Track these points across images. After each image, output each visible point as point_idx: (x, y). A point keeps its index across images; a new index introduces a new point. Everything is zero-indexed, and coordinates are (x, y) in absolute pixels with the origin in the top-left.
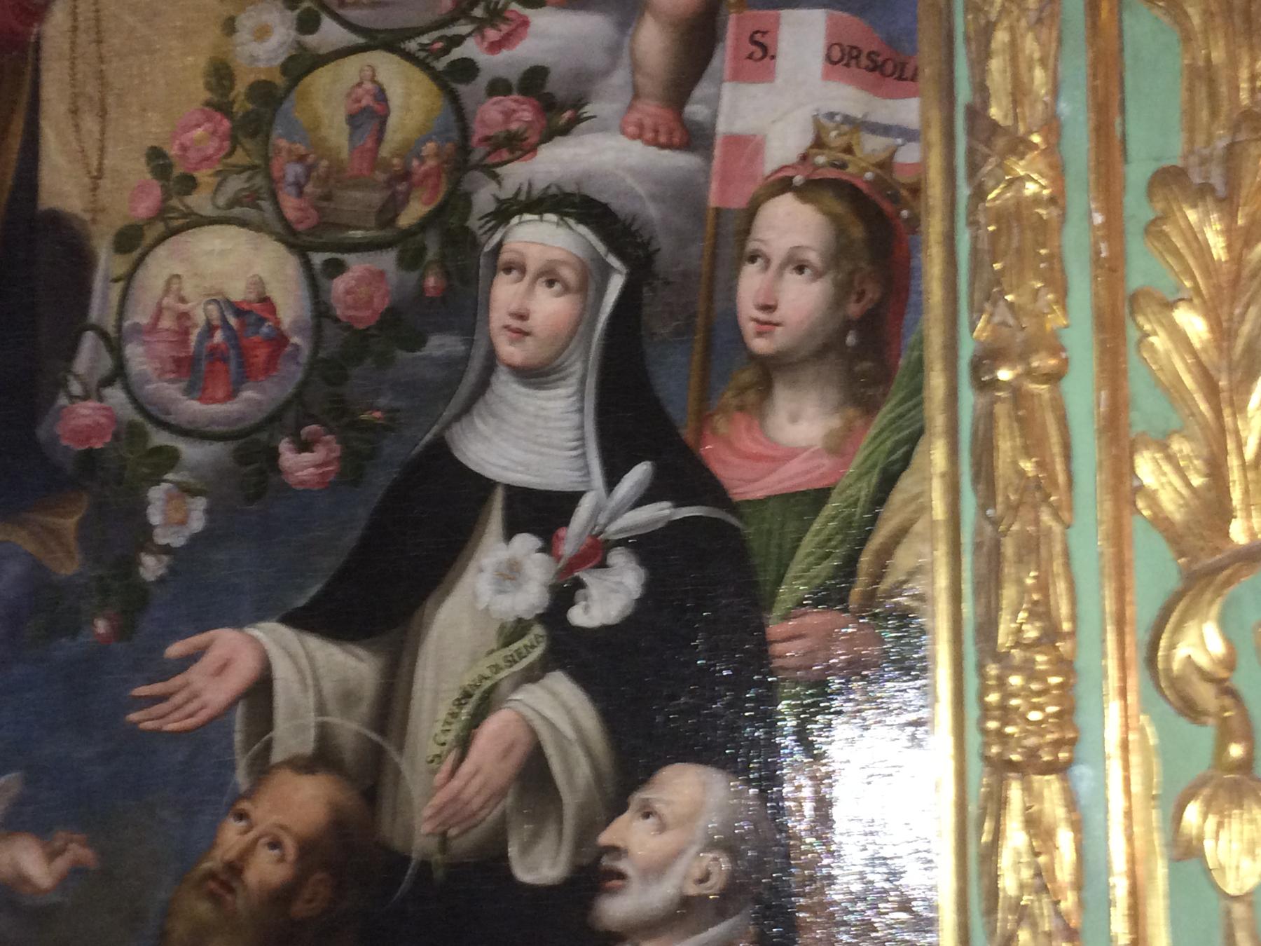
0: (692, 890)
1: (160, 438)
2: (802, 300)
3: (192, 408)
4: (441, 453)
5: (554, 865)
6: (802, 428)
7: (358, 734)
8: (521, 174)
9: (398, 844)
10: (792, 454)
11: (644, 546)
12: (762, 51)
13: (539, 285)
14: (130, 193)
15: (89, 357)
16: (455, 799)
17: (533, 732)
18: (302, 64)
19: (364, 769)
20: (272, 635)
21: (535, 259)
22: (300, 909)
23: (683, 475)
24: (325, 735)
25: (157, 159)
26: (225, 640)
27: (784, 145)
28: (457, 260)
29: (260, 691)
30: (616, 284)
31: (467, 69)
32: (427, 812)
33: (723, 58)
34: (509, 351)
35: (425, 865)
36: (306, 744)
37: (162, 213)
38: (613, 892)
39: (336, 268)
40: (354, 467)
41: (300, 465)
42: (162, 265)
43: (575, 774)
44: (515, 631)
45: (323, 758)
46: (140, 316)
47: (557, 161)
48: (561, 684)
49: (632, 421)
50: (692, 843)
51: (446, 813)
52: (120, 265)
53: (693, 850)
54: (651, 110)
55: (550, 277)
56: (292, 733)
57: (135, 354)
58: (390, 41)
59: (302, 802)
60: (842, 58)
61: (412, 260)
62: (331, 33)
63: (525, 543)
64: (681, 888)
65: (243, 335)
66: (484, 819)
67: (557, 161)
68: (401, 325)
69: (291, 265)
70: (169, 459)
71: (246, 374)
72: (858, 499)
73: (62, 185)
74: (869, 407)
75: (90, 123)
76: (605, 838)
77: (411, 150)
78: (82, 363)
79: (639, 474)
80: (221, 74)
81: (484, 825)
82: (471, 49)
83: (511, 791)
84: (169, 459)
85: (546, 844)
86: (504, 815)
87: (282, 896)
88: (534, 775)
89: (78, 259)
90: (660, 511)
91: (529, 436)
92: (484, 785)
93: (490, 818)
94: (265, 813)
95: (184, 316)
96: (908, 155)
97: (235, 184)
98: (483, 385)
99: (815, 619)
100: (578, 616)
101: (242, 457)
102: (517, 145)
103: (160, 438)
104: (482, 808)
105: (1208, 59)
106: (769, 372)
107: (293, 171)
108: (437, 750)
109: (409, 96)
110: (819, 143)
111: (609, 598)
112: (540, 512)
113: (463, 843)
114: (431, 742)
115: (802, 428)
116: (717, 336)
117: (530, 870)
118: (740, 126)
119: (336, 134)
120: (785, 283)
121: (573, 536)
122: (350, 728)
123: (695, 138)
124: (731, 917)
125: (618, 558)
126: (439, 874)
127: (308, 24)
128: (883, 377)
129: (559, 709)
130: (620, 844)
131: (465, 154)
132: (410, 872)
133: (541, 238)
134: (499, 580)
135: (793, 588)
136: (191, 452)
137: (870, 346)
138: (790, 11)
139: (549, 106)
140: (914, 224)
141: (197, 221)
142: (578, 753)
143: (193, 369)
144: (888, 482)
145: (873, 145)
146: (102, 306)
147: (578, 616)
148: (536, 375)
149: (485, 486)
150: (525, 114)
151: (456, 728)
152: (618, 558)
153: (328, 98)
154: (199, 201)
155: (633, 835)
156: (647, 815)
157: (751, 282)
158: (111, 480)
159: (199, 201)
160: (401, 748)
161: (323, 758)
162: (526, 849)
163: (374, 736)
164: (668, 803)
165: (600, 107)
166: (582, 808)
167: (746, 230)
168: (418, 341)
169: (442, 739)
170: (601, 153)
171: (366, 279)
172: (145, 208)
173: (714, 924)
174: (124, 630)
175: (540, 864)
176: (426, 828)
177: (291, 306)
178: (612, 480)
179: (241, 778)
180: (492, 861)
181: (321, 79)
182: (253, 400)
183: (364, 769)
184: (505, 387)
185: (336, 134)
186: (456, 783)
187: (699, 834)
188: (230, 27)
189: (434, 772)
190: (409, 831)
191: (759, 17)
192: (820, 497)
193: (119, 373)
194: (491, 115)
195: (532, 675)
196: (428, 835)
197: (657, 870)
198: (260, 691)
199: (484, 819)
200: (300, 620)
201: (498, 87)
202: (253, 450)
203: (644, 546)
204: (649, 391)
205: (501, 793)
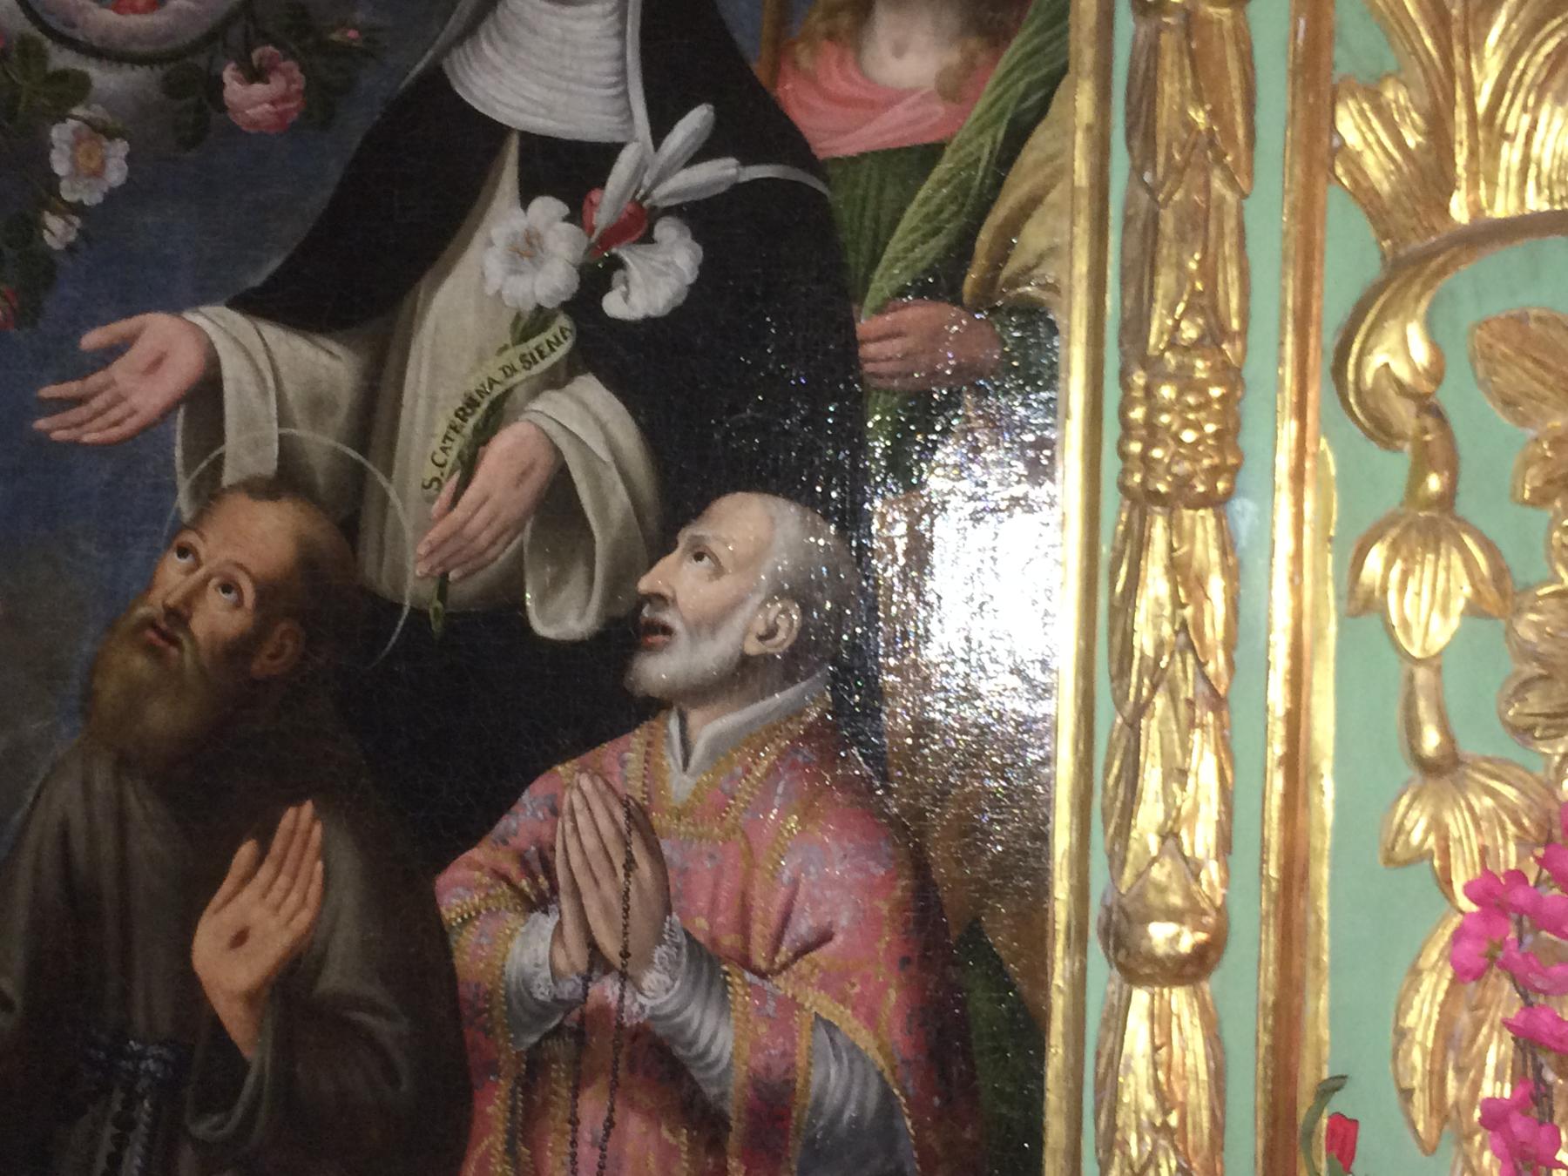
1: (61, 59)
10: (895, 97)
11: (699, 215)
19: (344, 498)
20: (219, 323)
23: (753, 124)
24: (288, 451)
26: (157, 328)
29: (205, 396)
36: (267, 461)
40: (323, 102)
41: (250, 99)
44: (534, 322)
45: (287, 480)
48: (590, 389)
56: (248, 448)
59: (263, 535)
63: (547, 209)
70: (78, 87)
74: (997, 37)
79: (695, 121)
84: (74, 88)
87: (238, 651)
88: (556, 505)
90: (722, 171)
99: (917, 313)
100: (614, 305)
101: (173, 88)
103: (61, 59)
111: (655, 281)
112: (567, 169)
121: (608, 202)
122: (322, 444)
125: (667, 231)
129: (589, 422)
134: (513, 257)
136: (104, 78)
147: (614, 305)
149: (496, 132)
152: (667, 231)
155: (680, 580)
161: (287, 480)
175: (564, 615)
178: (660, 131)
179: (184, 504)
180: (503, 611)
192: (930, 154)
195: (555, 380)
197: (710, 624)
198: (205, 396)
200: (253, 304)
203: (699, 215)
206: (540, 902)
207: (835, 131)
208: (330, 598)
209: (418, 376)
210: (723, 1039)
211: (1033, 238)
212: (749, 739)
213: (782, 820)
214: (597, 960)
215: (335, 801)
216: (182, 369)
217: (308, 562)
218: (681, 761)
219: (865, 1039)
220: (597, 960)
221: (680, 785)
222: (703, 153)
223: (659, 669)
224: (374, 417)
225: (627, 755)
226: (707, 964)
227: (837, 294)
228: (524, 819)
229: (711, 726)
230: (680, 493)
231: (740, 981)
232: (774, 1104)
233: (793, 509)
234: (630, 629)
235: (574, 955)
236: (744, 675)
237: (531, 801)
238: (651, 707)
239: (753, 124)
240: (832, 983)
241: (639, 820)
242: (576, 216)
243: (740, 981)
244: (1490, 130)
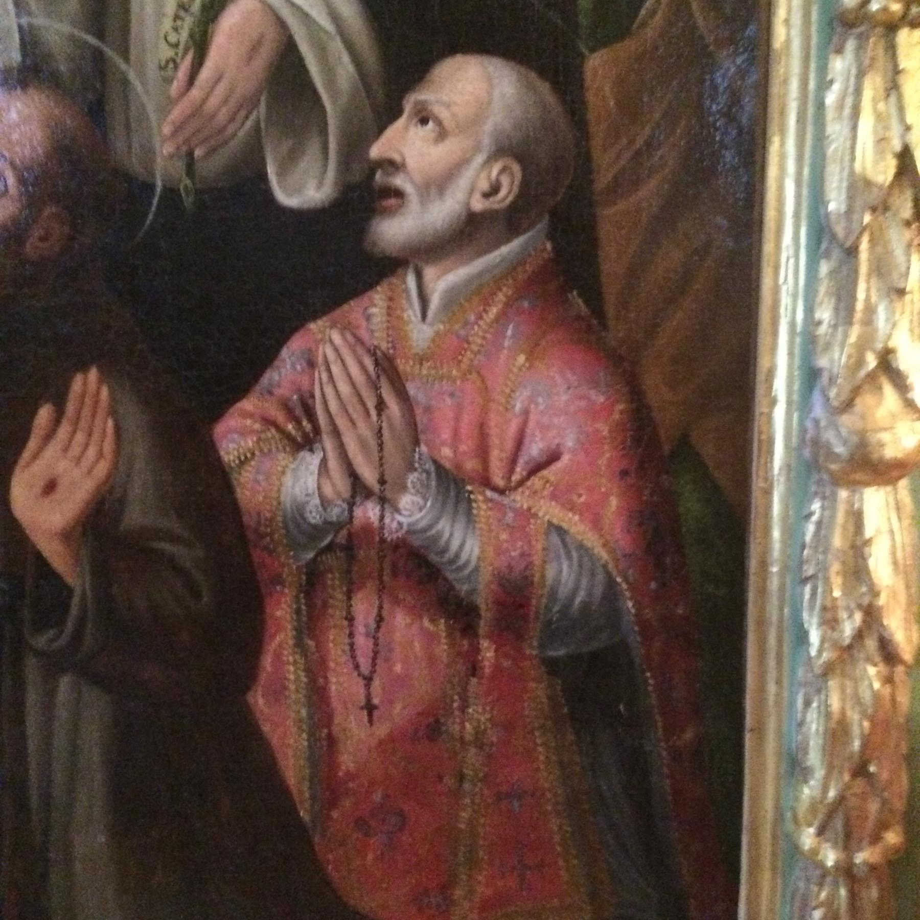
0: (478, 205)
5: (320, 185)
7: (72, 38)
9: (135, 166)
16: (197, 111)
17: (282, 24)
22: (32, 247)
32: (167, 130)
35: (171, 193)
38: (389, 212)
43: (335, 75)
47: (852, 791)
50: (477, 149)
51: (189, 130)
53: (480, 159)
64: (468, 204)
66: (234, 135)
72: (127, 60)
76: (376, 151)
81: (232, 143)
83: (263, 99)
85: (309, 162)
86: (257, 129)
88: (286, 78)
92: (231, 91)
93: (241, 134)
104: (232, 120)
108: (169, 53)
113: (211, 166)
114: (163, 44)
117: (289, 194)
124: (525, 231)
126: (188, 202)
130: (397, 157)
132: (155, 201)
142: (337, 46)
151: (188, 23)
155: (409, 146)
156: (424, 121)
160: (125, 53)
162: (289, 162)
163: (92, 40)
164: (448, 106)
166: (347, 118)
169: (173, 38)
173: (508, 240)
175: (304, 186)
176: (167, 149)
180: (246, 185)
186: (196, 93)
187: (487, 141)
189: (169, 81)
190: (149, 153)
196: (171, 157)
197: (438, 185)
199: (234, 135)
205: (251, 103)
206: (306, 442)
210: (471, 547)
214: (359, 489)
217: (63, 151)
218: (419, 312)
219: (592, 540)
221: (421, 334)
223: (394, 230)
225: (376, 302)
226: (452, 486)
228: (285, 371)
229: (443, 280)
231: (481, 500)
234: (366, 193)
235: (339, 484)
236: (470, 232)
238: (387, 266)
241: (386, 368)
243: (481, 500)
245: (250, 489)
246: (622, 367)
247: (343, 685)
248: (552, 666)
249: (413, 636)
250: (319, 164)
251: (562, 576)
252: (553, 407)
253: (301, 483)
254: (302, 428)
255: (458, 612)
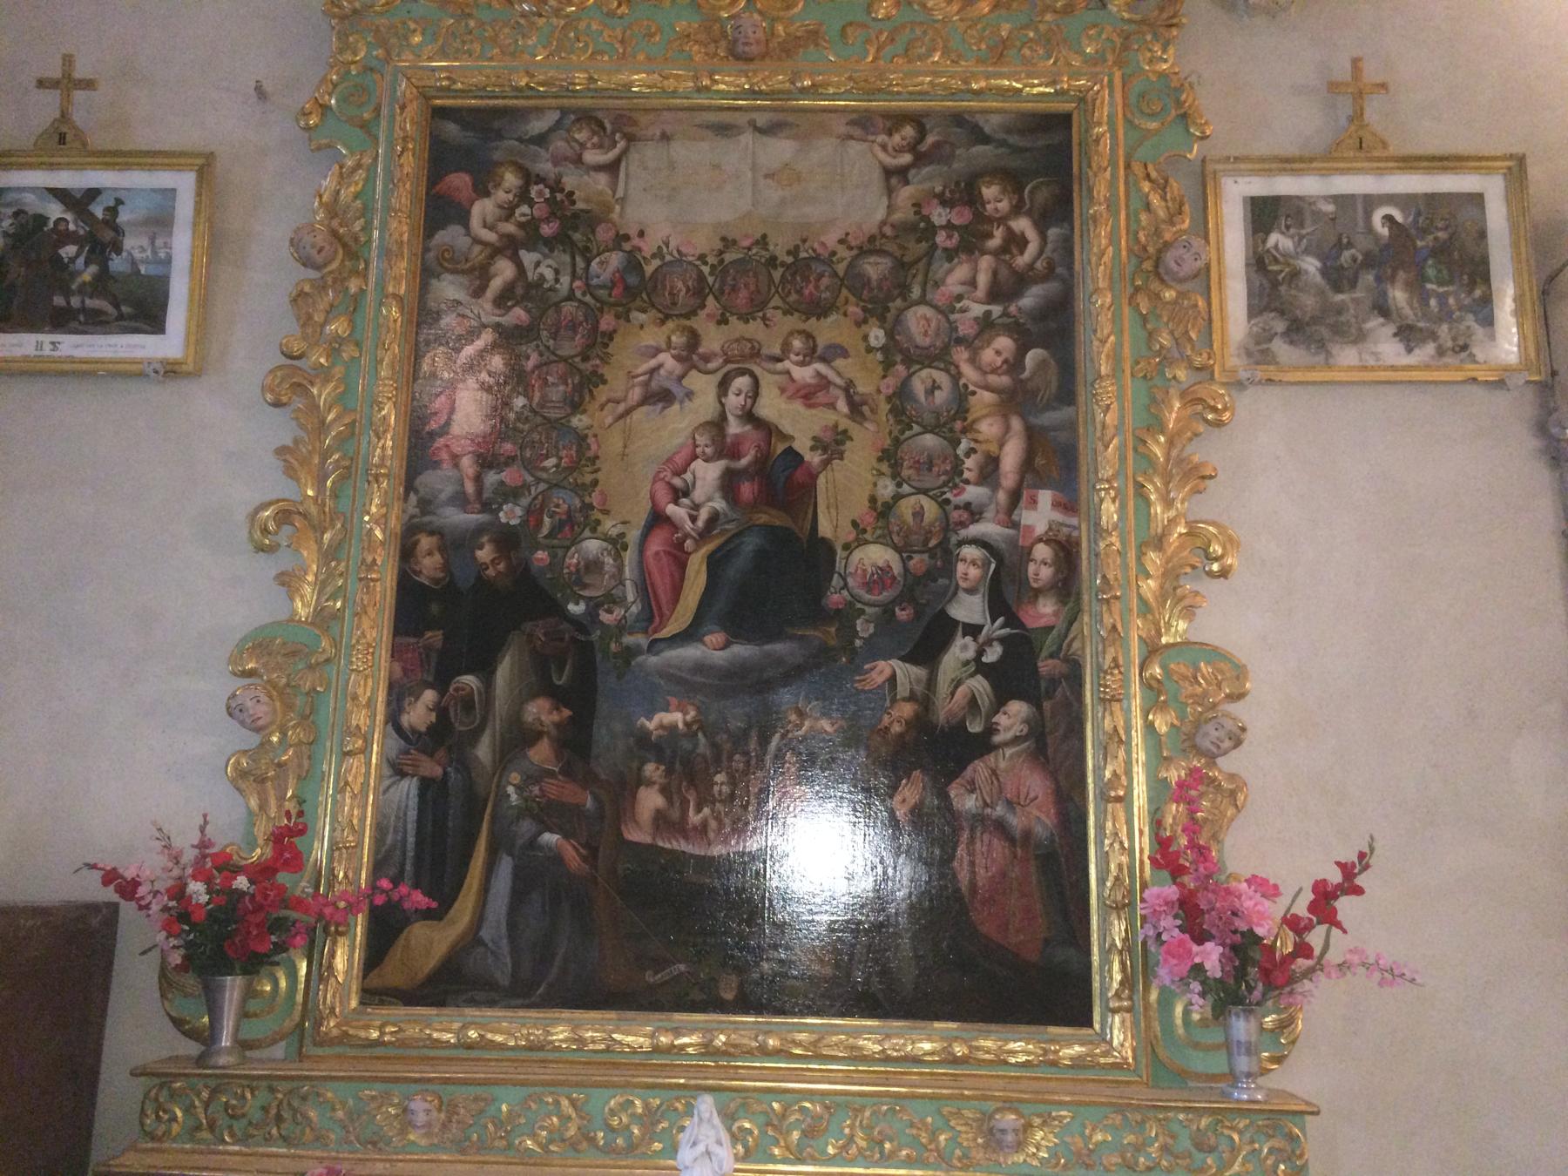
1: (859, 606)
2: (1046, 573)
3: (868, 597)
4: (943, 613)
6: (1046, 610)
8: (964, 533)
10: (1043, 616)
11: (1002, 640)
12: (1034, 502)
13: (970, 565)
14: (847, 534)
15: (836, 579)
18: (898, 497)
19: (924, 699)
20: (895, 663)
21: (969, 558)
23: (1013, 620)
24: (911, 690)
25: (855, 524)
26: (881, 664)
27: (1041, 528)
28: (946, 556)
29: (893, 679)
30: (993, 566)
31: (947, 501)
33: (1022, 503)
34: (962, 584)
36: (907, 694)
37: (857, 539)
39: (910, 558)
40: (918, 615)
41: (902, 615)
42: (857, 555)
44: (966, 663)
45: (912, 698)
46: (851, 569)
47: (975, 530)
48: (979, 677)
49: (998, 605)
52: (845, 554)
54: (1002, 516)
55: (974, 563)
56: (903, 690)
57: (849, 580)
58: (925, 492)
59: (907, 710)
60: (1056, 505)
61: (932, 557)
62: (906, 488)
63: (968, 639)
65: (881, 578)
67: (975, 530)
68: (930, 575)
69: (897, 556)
70: (862, 612)
71: (884, 588)
73: (825, 528)
74: (1065, 604)
75: (833, 511)
77: (932, 524)
78: (834, 582)
79: (1000, 620)
80: (873, 500)
82: (948, 495)
84: (862, 612)
87: (901, 735)
88: (973, 702)
89: (831, 551)
90: (1007, 630)
91: (969, 609)
94: (895, 713)
95: (865, 571)
96: (1075, 534)
97: (879, 532)
98: (955, 594)
99: (1050, 661)
100: (984, 659)
101: (885, 612)
102: (963, 525)
103: (859, 606)
105: (991, 11)
106: (1037, 593)
107: (896, 529)
109: (930, 509)
110: (1050, 529)
111: (993, 655)
112: (973, 630)
115: (1046, 610)
116: (1022, 581)
118: (1029, 522)
119: (909, 519)
120: (1041, 570)
121: (981, 639)
122: (919, 689)
123: (1015, 525)
125: (995, 643)
127: (899, 485)
128: (1069, 595)
129: (980, 685)
131: (947, 527)
133: (970, 552)
134: (961, 649)
135: (1044, 654)
136: (868, 610)
137: (1067, 584)
138: (96, 1142)
139: (972, 514)
140: (1078, 552)
141: (867, 542)
143: (869, 586)
144: (1071, 624)
145: (1065, 530)
146: (839, 566)
147: (984, 659)
148: (971, 591)
149: (957, 622)
150: (966, 516)
152: (995, 643)
153: (906, 508)
154: (868, 536)
155: (1001, 719)
157: (1032, 568)
158: (845, 617)
159: (868, 536)
161: (912, 698)
165: (989, 514)
167: (1029, 553)
168: (935, 580)
170: (987, 528)
171: (919, 562)
172: (852, 537)
174: (851, 661)
175: (975, 727)
177: (897, 568)
178: (993, 621)
179: (888, 703)
180: (962, 726)
181: (903, 502)
182: (886, 596)
183: (924, 699)
184: (961, 594)
185: (909, 519)
188: (875, 485)
191: (1032, 491)
192: (1053, 628)
193: (846, 586)
194: (955, 515)
195: (972, 675)
197: (1008, 729)
198: (893, 679)
200: (903, 659)
201: (957, 507)
202: (887, 610)
203: (1002, 640)
204: (1006, 588)
206: (972, 791)
207: (1031, 624)
208: (922, 723)
209: (941, 677)
210: (1016, 822)
211: (1076, 645)
212: (1018, 754)
213: (1026, 772)
214: (986, 805)
215: (924, 769)
216: (888, 672)
217: (917, 717)
218: (1003, 760)
219: (1048, 822)
220: (986, 805)
221: (1002, 765)
222: (1002, 627)
223: (997, 739)
224: (931, 682)
225: (992, 757)
226: (1010, 804)
227: (1033, 656)
228: (969, 772)
229: (1009, 752)
230: (1000, 702)
231: (1018, 808)
232: (1027, 834)
233: (841, 887)
234: (991, 730)
235: (980, 803)
236: (1016, 740)
237: (970, 768)
238: (996, 747)
239: (1013, 620)
240: (1039, 808)
241: (994, 772)
242: (975, 640)
243: (1018, 808)
244: (1168, 625)
245: (956, 804)
246: (1053, 775)
247: (979, 860)
248: (1037, 857)
249: (999, 847)
250: (1561, 276)
251: (1038, 830)
252: (1036, 784)
253: (969, 804)
254: (972, 788)
255: (1011, 840)
